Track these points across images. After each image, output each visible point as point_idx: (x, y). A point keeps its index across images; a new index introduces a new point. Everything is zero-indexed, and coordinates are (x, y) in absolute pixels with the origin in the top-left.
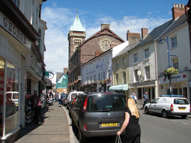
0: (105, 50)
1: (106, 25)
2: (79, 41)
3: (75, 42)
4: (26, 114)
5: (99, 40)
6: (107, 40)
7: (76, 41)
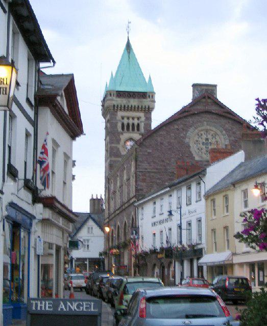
3: (123, 125)
6: (208, 127)
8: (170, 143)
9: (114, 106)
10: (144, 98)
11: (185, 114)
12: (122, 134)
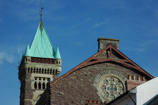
0: (110, 99)
1: (109, 42)
2: (42, 81)
3: (35, 84)
4: (96, 89)
5: (93, 75)
6: (112, 75)
7: (38, 81)
8: (79, 87)
9: (29, 68)
10: (53, 63)
11: (93, 62)
12: (35, 91)
